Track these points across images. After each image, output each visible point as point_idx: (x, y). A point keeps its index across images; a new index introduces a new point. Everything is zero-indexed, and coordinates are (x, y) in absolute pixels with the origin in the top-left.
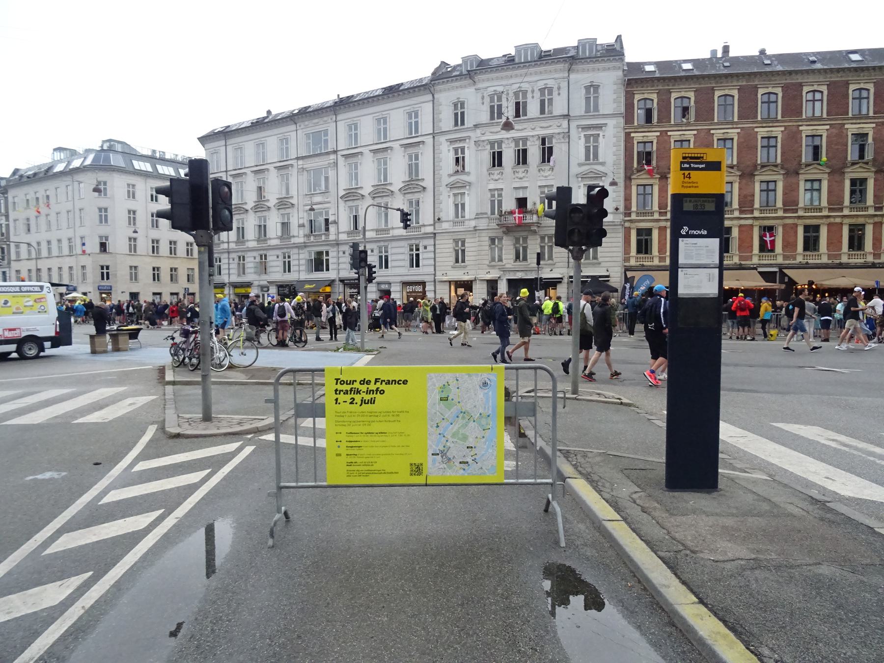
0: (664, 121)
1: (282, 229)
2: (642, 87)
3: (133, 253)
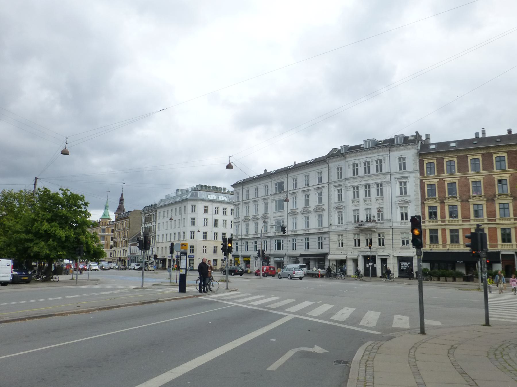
0: (440, 173)
1: (457, 213)
2: (428, 157)
3: (215, 240)
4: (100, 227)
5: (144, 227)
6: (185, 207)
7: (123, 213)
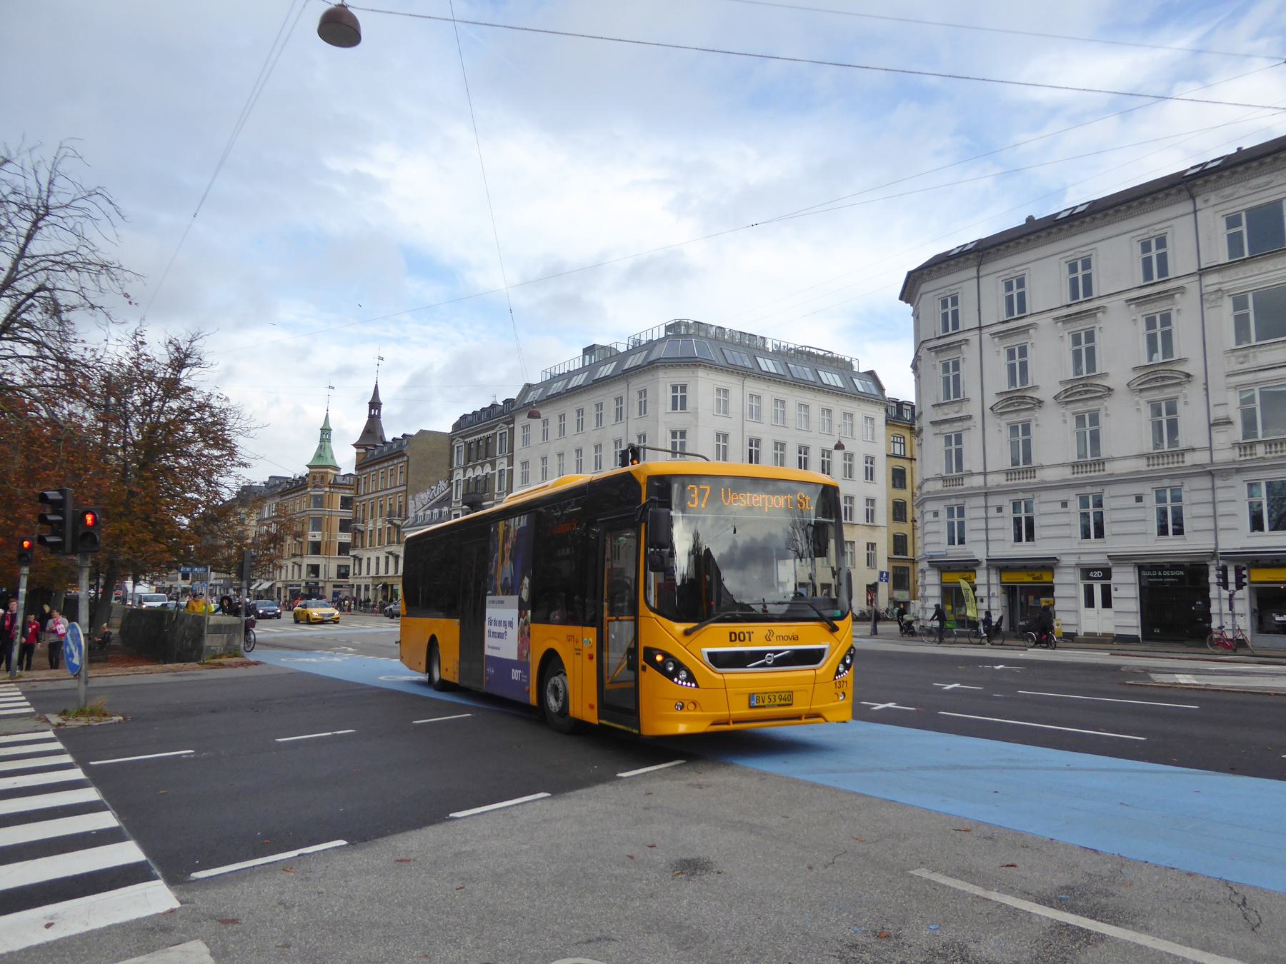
4: (309, 489)
5: (462, 479)
6: (643, 393)
7: (375, 446)
